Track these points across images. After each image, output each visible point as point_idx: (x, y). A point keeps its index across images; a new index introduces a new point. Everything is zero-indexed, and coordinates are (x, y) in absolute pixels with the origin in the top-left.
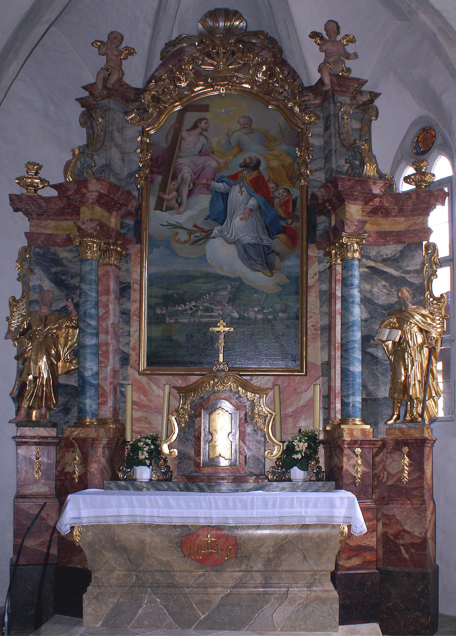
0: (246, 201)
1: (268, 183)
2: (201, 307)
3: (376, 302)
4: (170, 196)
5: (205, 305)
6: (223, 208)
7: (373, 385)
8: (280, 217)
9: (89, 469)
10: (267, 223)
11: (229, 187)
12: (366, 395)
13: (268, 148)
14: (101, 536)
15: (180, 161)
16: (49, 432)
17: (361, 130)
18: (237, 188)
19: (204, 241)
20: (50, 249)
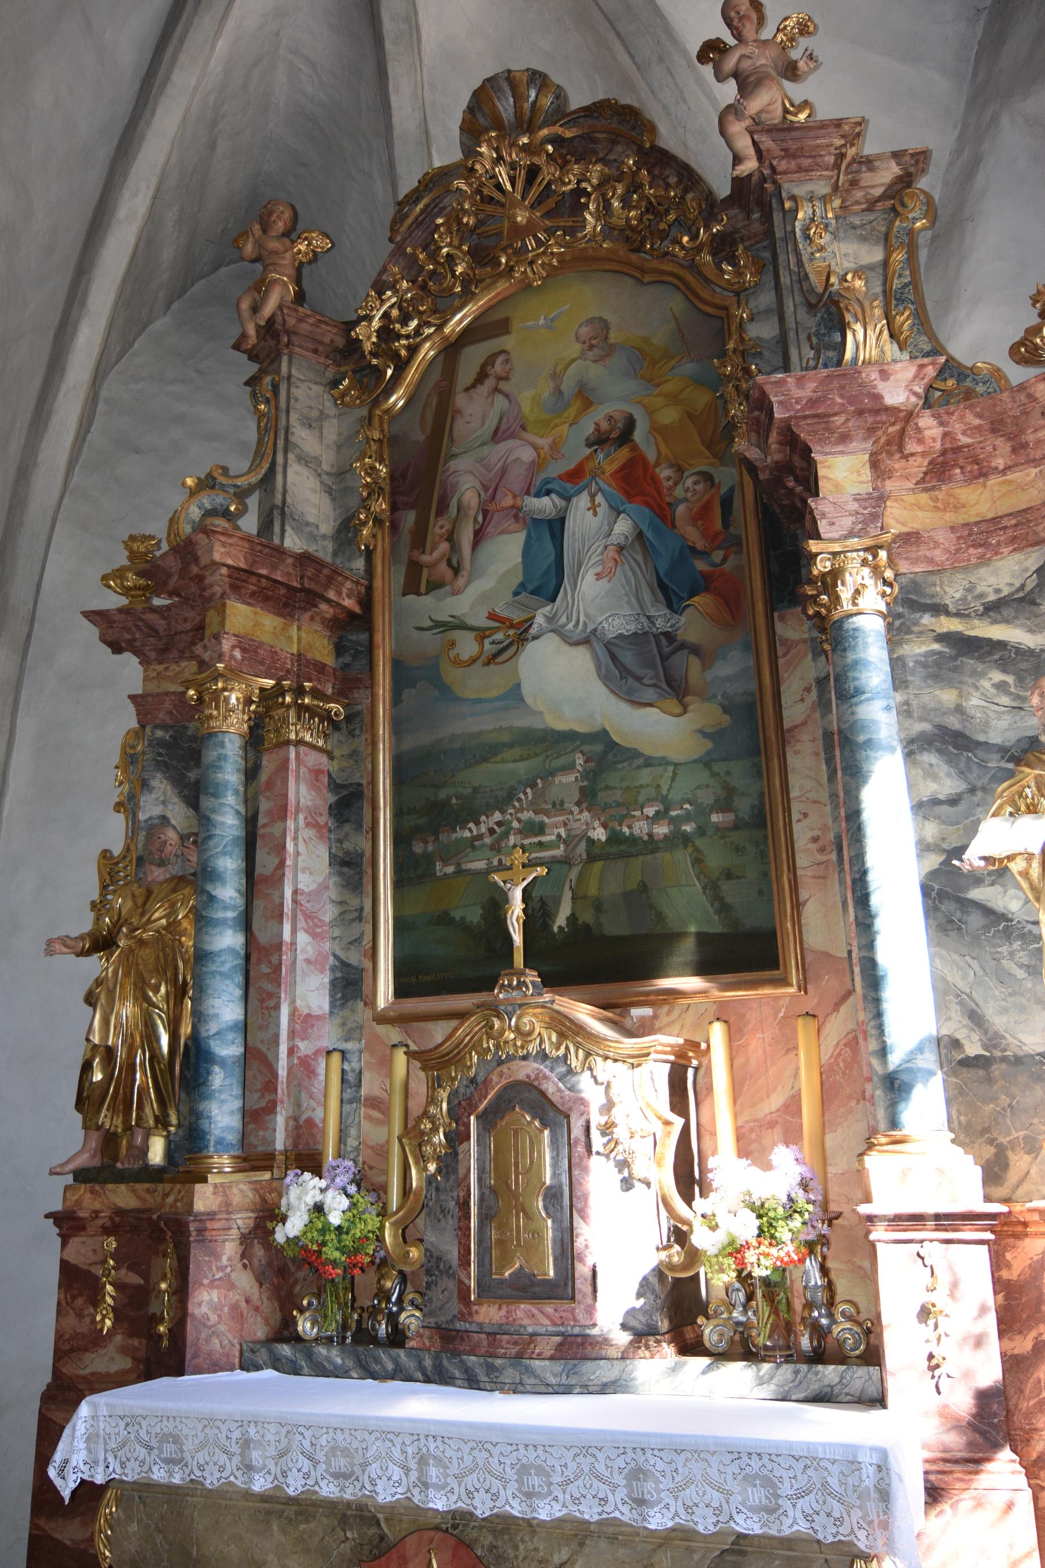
0: (606, 528)
1: (657, 470)
2: (515, 824)
3: (981, 738)
4: (436, 554)
5: (526, 815)
6: (552, 557)
7: (1004, 1011)
8: (693, 550)
9: (192, 1308)
10: (662, 576)
11: (564, 503)
12: (985, 1047)
13: (649, 381)
14: (159, 1539)
15: (453, 465)
16: (139, 1198)
17: (886, 263)
18: (582, 501)
19: (514, 648)
20: (187, 728)
